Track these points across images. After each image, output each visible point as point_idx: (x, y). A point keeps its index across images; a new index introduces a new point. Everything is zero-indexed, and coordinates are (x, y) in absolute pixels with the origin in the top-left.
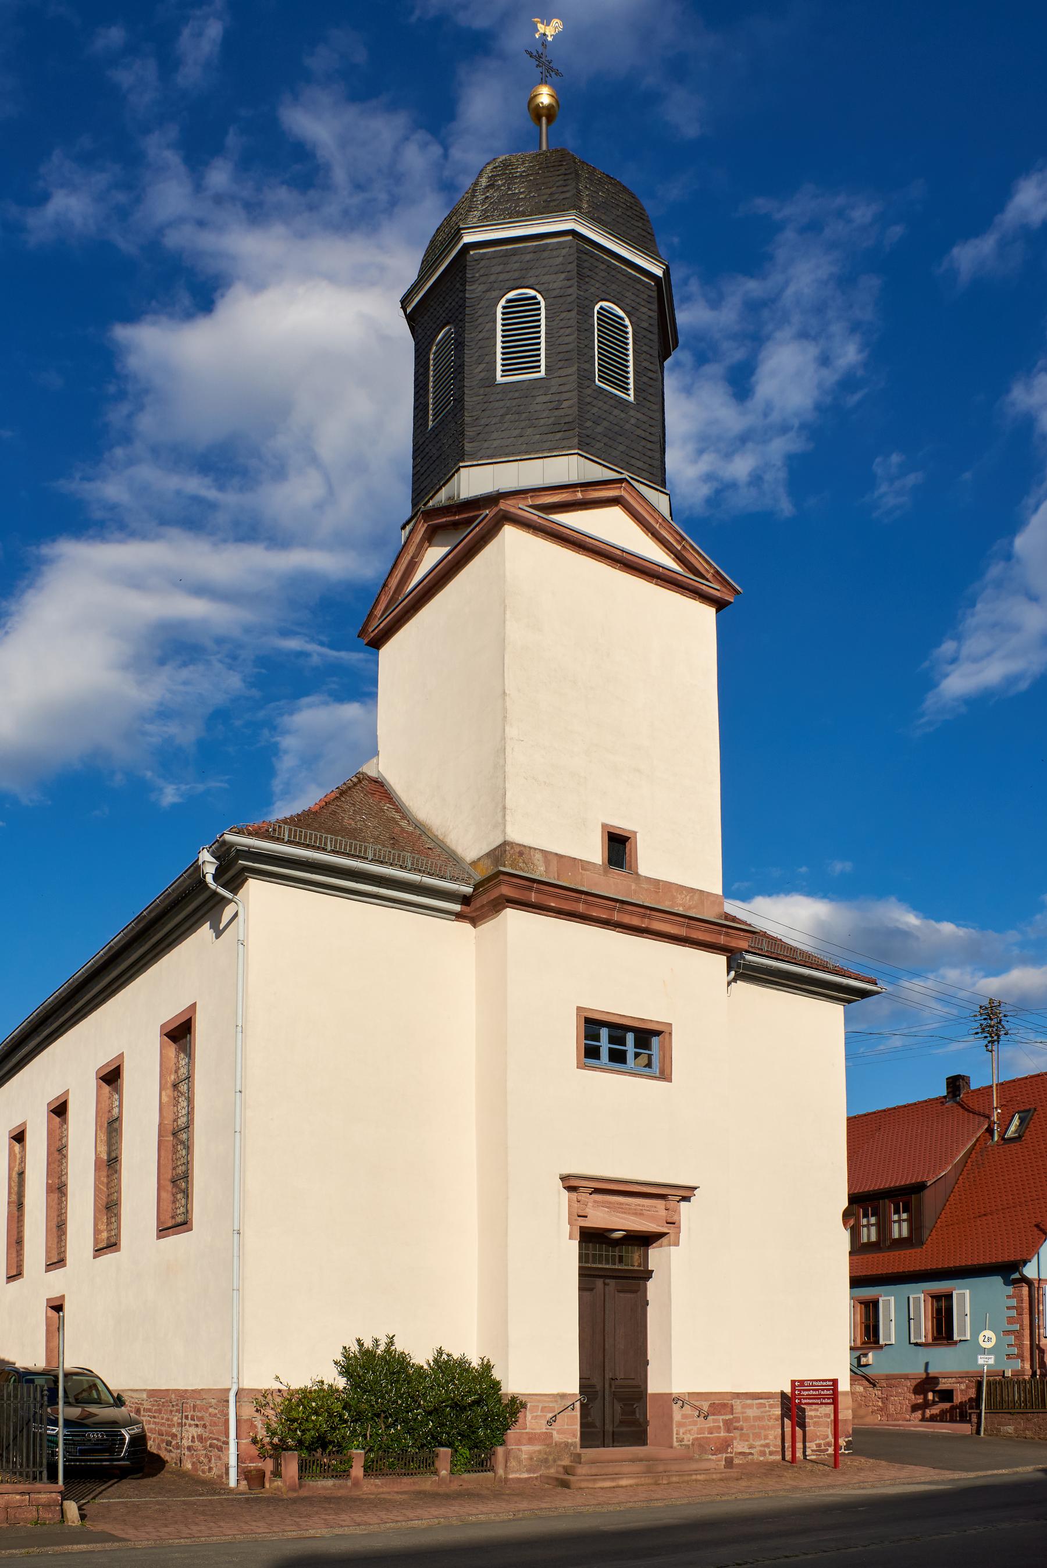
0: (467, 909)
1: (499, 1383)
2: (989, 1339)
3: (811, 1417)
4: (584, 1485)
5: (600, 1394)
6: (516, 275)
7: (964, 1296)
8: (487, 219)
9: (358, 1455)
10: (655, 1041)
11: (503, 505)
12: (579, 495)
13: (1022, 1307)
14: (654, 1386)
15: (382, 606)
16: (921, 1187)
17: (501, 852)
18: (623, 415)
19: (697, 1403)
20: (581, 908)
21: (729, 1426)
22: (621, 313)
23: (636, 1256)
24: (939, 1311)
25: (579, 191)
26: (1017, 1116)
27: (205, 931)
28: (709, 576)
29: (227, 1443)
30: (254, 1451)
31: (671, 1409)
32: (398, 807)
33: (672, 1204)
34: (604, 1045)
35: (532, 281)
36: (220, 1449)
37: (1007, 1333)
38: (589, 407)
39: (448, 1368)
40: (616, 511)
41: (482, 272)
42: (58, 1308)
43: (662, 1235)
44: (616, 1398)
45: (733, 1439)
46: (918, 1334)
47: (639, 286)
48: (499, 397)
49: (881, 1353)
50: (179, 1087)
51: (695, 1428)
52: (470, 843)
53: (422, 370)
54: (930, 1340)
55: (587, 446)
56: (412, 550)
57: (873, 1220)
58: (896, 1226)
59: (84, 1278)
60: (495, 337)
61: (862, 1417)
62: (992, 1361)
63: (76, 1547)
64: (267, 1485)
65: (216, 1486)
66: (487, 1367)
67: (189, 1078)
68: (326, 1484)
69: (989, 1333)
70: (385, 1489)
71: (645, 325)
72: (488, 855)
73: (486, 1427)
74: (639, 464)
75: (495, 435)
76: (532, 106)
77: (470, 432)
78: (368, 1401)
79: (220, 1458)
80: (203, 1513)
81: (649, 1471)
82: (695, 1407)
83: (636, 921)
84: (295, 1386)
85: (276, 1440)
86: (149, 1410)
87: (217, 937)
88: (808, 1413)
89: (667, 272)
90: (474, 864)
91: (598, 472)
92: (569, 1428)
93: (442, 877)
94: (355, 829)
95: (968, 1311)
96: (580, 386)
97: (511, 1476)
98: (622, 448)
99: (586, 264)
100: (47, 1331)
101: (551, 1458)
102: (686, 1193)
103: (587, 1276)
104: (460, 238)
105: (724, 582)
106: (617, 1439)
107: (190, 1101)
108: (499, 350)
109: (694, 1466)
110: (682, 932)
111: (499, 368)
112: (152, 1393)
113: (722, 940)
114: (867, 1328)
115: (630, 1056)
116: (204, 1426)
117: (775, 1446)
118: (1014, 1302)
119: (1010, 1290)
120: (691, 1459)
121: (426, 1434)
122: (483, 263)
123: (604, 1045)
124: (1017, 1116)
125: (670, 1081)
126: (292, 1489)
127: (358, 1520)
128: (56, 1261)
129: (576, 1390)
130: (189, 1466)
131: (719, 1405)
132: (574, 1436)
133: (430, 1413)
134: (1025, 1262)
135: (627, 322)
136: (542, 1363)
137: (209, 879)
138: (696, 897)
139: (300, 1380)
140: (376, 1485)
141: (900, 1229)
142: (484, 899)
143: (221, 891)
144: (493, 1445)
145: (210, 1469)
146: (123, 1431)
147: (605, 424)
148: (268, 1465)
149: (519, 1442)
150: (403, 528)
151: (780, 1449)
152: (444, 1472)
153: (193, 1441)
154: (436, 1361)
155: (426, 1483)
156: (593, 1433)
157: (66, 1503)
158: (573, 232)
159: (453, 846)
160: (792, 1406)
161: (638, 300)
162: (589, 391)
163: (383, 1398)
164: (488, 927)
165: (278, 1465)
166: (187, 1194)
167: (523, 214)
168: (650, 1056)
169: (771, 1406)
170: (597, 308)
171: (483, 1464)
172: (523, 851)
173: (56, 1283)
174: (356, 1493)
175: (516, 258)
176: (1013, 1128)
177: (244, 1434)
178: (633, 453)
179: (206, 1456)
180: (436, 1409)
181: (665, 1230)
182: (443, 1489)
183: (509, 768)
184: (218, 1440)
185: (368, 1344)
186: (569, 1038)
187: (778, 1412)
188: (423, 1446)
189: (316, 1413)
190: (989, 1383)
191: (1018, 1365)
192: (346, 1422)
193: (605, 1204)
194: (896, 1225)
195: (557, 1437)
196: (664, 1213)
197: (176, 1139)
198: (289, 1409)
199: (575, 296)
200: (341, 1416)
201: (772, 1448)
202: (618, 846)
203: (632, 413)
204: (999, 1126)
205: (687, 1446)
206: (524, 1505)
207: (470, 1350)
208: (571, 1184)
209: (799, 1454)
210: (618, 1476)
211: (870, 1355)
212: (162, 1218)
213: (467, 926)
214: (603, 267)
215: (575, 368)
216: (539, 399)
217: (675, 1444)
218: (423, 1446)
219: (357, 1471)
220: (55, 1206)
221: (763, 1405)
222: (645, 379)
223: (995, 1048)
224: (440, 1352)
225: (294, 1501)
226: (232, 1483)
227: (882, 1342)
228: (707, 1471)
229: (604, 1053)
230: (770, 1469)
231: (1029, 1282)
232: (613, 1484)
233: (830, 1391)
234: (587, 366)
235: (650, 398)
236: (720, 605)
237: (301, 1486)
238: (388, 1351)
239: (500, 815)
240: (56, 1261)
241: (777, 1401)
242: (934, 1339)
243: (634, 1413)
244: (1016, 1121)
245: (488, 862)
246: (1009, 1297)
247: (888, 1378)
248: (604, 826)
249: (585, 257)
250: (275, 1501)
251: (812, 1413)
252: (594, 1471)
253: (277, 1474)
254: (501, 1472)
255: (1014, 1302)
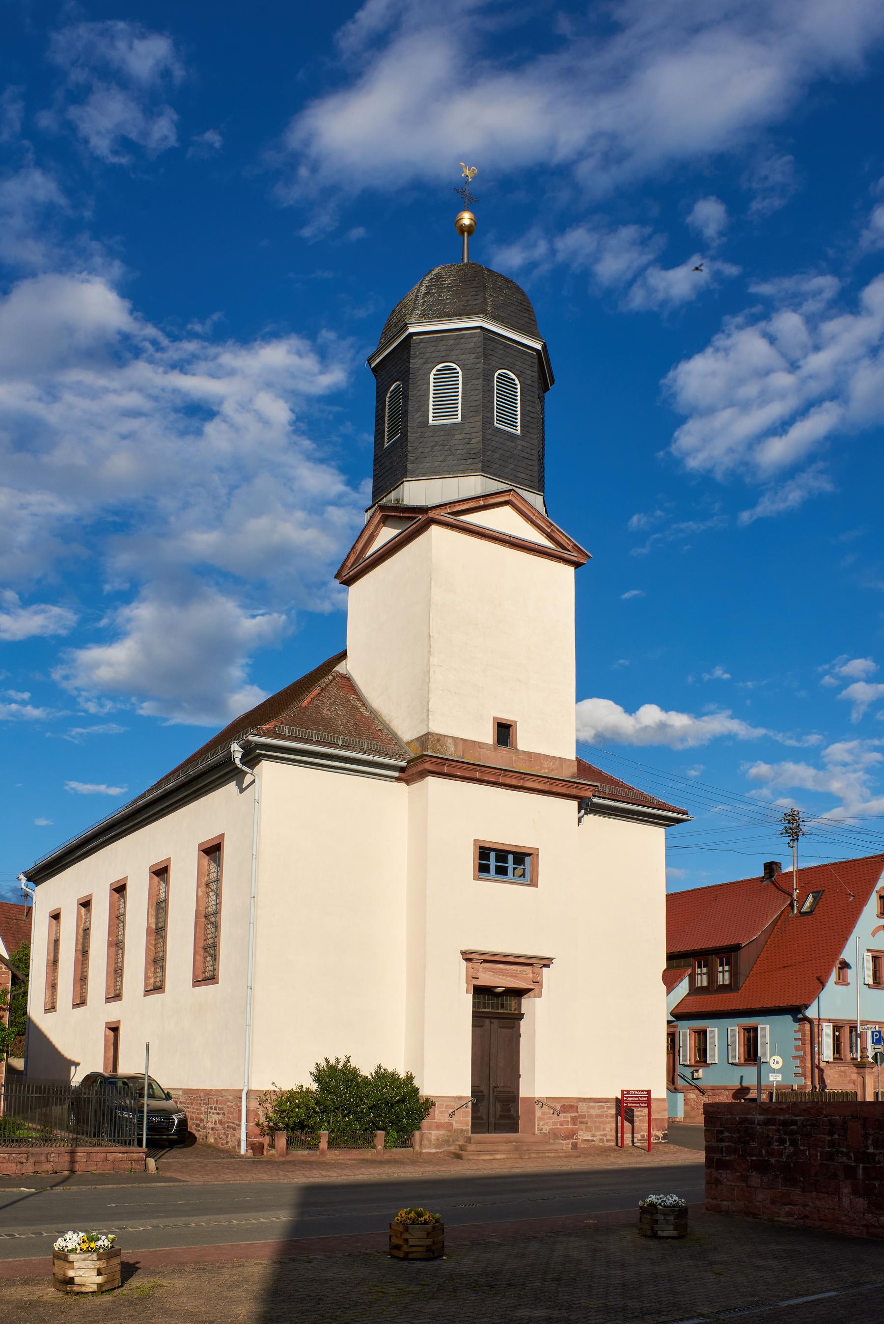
0: (403, 775)
1: (417, 1089)
2: (778, 1062)
3: (638, 1116)
4: (471, 1157)
5: (486, 1097)
6: (443, 354)
7: (766, 1028)
8: (426, 316)
9: (324, 1134)
10: (527, 859)
11: (431, 514)
12: (482, 503)
13: (805, 1039)
14: (523, 1093)
15: (351, 560)
16: (737, 948)
17: (425, 739)
18: (513, 444)
19: (552, 1105)
20: (478, 775)
21: (574, 1120)
22: (513, 376)
23: (513, 1003)
24: (749, 1039)
25: (485, 298)
26: (811, 896)
27: (232, 786)
28: (569, 548)
29: (240, 1125)
30: (257, 1130)
31: (534, 1107)
32: (360, 698)
33: (537, 970)
34: (493, 863)
35: (453, 358)
36: (234, 1129)
37: (795, 1057)
38: (489, 442)
39: (384, 1078)
40: (507, 509)
41: (421, 351)
42: (115, 1029)
43: (530, 990)
44: (497, 1099)
45: (578, 1130)
46: (734, 1057)
47: (525, 357)
48: (431, 434)
49: (706, 1069)
50: (210, 886)
51: (551, 1122)
52: (407, 730)
53: (380, 407)
54: (742, 1061)
55: (487, 469)
56: (372, 528)
57: (705, 970)
58: (721, 975)
59: (135, 1010)
60: (429, 395)
61: (694, 1117)
62: (779, 1079)
63: (158, 1184)
64: (265, 1153)
65: (232, 1153)
66: (410, 1078)
67: (218, 880)
68: (303, 1153)
69: (777, 1058)
70: (341, 1157)
71: (529, 382)
72: (417, 739)
73: (409, 1118)
74: (523, 476)
75: (427, 459)
76: (458, 225)
77: (411, 457)
78: (332, 1099)
79: (234, 1135)
80: (228, 1168)
81: (516, 1149)
82: (551, 1107)
83: (514, 782)
84: (286, 1087)
85: (271, 1124)
86: (184, 1103)
87: (241, 792)
88: (636, 1113)
89: (544, 347)
90: (408, 743)
91: (495, 486)
92: (464, 1120)
93: (387, 755)
94: (331, 719)
95: (716, 1043)
96: (484, 428)
97: (424, 1151)
98: (512, 466)
99: (490, 347)
100: (105, 1045)
101: (451, 1139)
102: (547, 962)
103: (478, 1018)
104: (407, 329)
105: (580, 551)
106: (498, 1128)
107: (218, 895)
108: (431, 403)
109: (548, 1147)
110: (546, 787)
111: (431, 415)
112: (186, 1091)
113: (574, 792)
114: (699, 1050)
115: (510, 871)
116: (224, 1114)
117: (611, 1136)
118: (799, 1035)
119: (797, 1026)
120: (547, 1143)
121: (369, 1122)
122: (422, 345)
123: (493, 863)
124: (811, 896)
125: (537, 887)
126: (282, 1155)
127: (324, 1174)
128: (115, 996)
129: (468, 1093)
130: (212, 1141)
131: (568, 1106)
132: (467, 1125)
133: (371, 1108)
134: (806, 1007)
135: (517, 382)
136: (446, 1075)
137: (237, 761)
138: (558, 762)
139: (288, 1084)
140: (335, 1155)
141: (724, 978)
142: (414, 770)
143: (245, 768)
144: (412, 1130)
145: (227, 1143)
146: (174, 1116)
147: (501, 451)
148: (266, 1140)
149: (430, 1128)
150: (366, 511)
151: (614, 1138)
152: (379, 1147)
153: (215, 1124)
154: (376, 1073)
155: (368, 1154)
156: (480, 1123)
157: (148, 1159)
158: (481, 328)
159: (395, 729)
160: (625, 1108)
161: (525, 366)
162: (490, 431)
163: (341, 1097)
164: (416, 786)
165: (273, 1140)
166: (215, 958)
167: (449, 316)
168: (524, 870)
169: (608, 1108)
170: (496, 374)
171: (406, 1143)
172: (440, 739)
173: (114, 1012)
174: (322, 1159)
175: (444, 343)
176: (808, 904)
177: (251, 1119)
178: (519, 469)
179: (225, 1134)
180: (374, 1106)
181: (532, 987)
182: (379, 1158)
183: (431, 684)
184: (233, 1123)
185: (332, 1061)
186: (469, 860)
187: (613, 1111)
188: (366, 1129)
189: (298, 1106)
190: (777, 1095)
191: (802, 1081)
192: (317, 1113)
193: (490, 970)
194: (721, 975)
195: (455, 1125)
196: (531, 975)
197: (208, 921)
198: (280, 1104)
199: (480, 370)
200: (314, 1109)
201: (608, 1137)
202: (504, 731)
203: (519, 442)
204: (798, 902)
205: (545, 1134)
206: (430, 1168)
207: (398, 1065)
208: (468, 957)
209: (628, 1141)
210: (495, 1152)
211: (701, 1071)
212: (197, 973)
213: (403, 785)
214: (501, 347)
215: (480, 417)
216: (457, 437)
217: (537, 1132)
218: (366, 1129)
219: (324, 1145)
220: (114, 957)
221: (603, 1107)
222: (528, 419)
223: (795, 845)
224: (380, 1067)
225: (284, 1163)
226: (243, 1152)
227: (709, 1062)
228: (556, 1151)
229: (493, 869)
230: (604, 1151)
231: (810, 1021)
232: (492, 1157)
233: (646, 1098)
234: (489, 415)
235: (531, 430)
236: (577, 565)
237: (287, 1154)
238: (345, 1066)
239: (426, 714)
240: (115, 996)
241: (614, 1104)
242: (746, 1060)
243: (510, 1110)
244: (810, 899)
245: (417, 744)
246: (796, 1031)
247: (713, 1088)
248: (495, 718)
249: (489, 342)
250: (270, 1162)
251: (638, 1113)
252: (479, 1148)
253: (272, 1146)
254: (417, 1148)
255: (799, 1035)
